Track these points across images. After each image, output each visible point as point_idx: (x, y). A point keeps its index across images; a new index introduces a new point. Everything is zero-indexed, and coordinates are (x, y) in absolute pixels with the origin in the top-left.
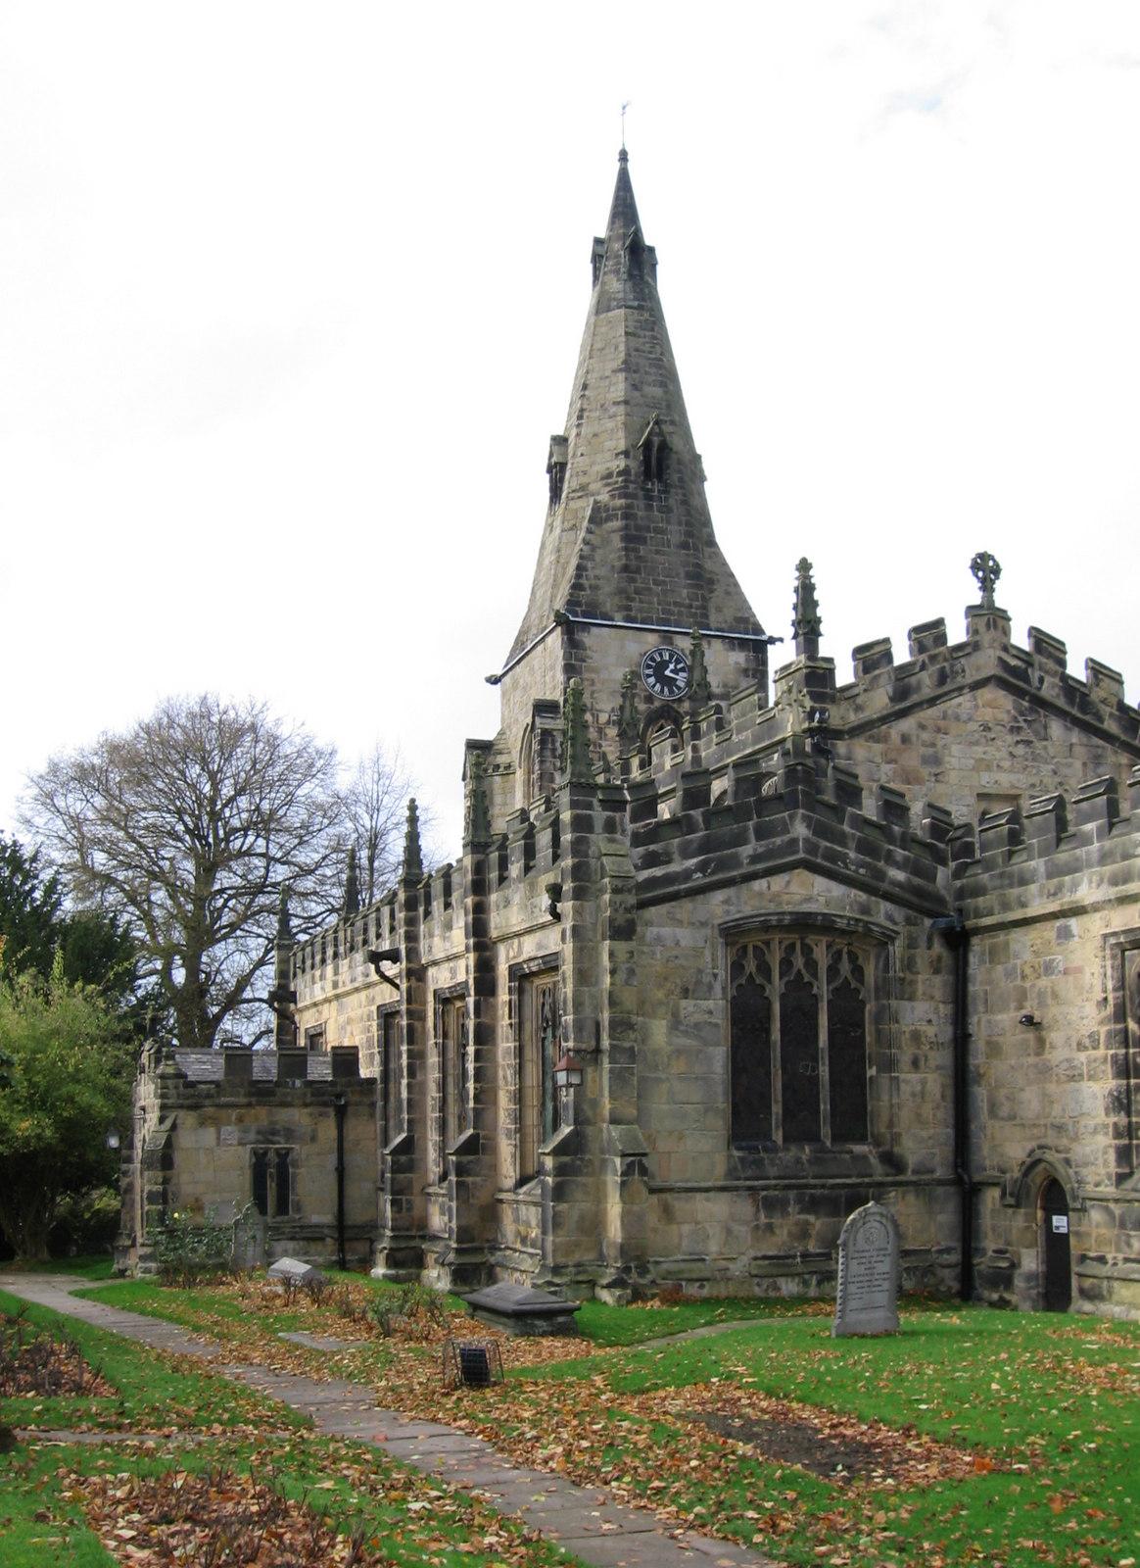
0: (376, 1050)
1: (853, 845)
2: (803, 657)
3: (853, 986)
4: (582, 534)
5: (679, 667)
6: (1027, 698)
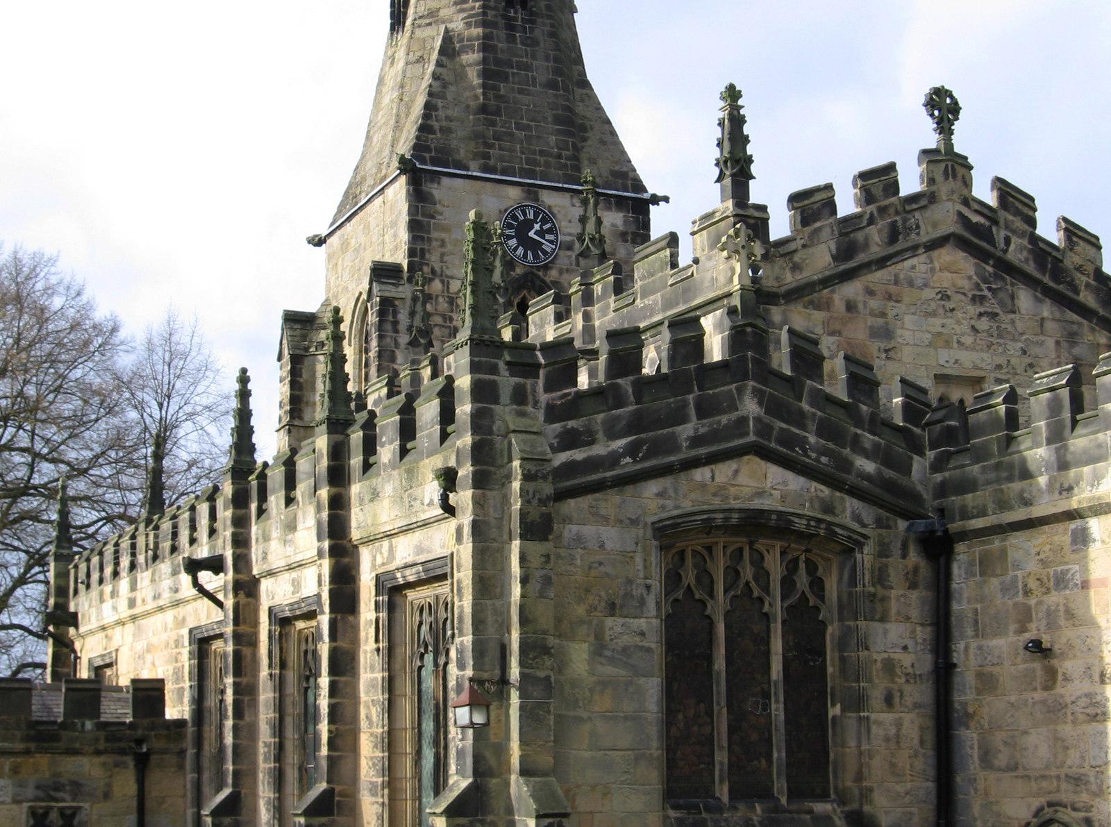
0: (187, 684)
1: (812, 427)
2: (730, 204)
3: (811, 604)
4: (431, 68)
5: (545, 227)
6: (991, 262)
